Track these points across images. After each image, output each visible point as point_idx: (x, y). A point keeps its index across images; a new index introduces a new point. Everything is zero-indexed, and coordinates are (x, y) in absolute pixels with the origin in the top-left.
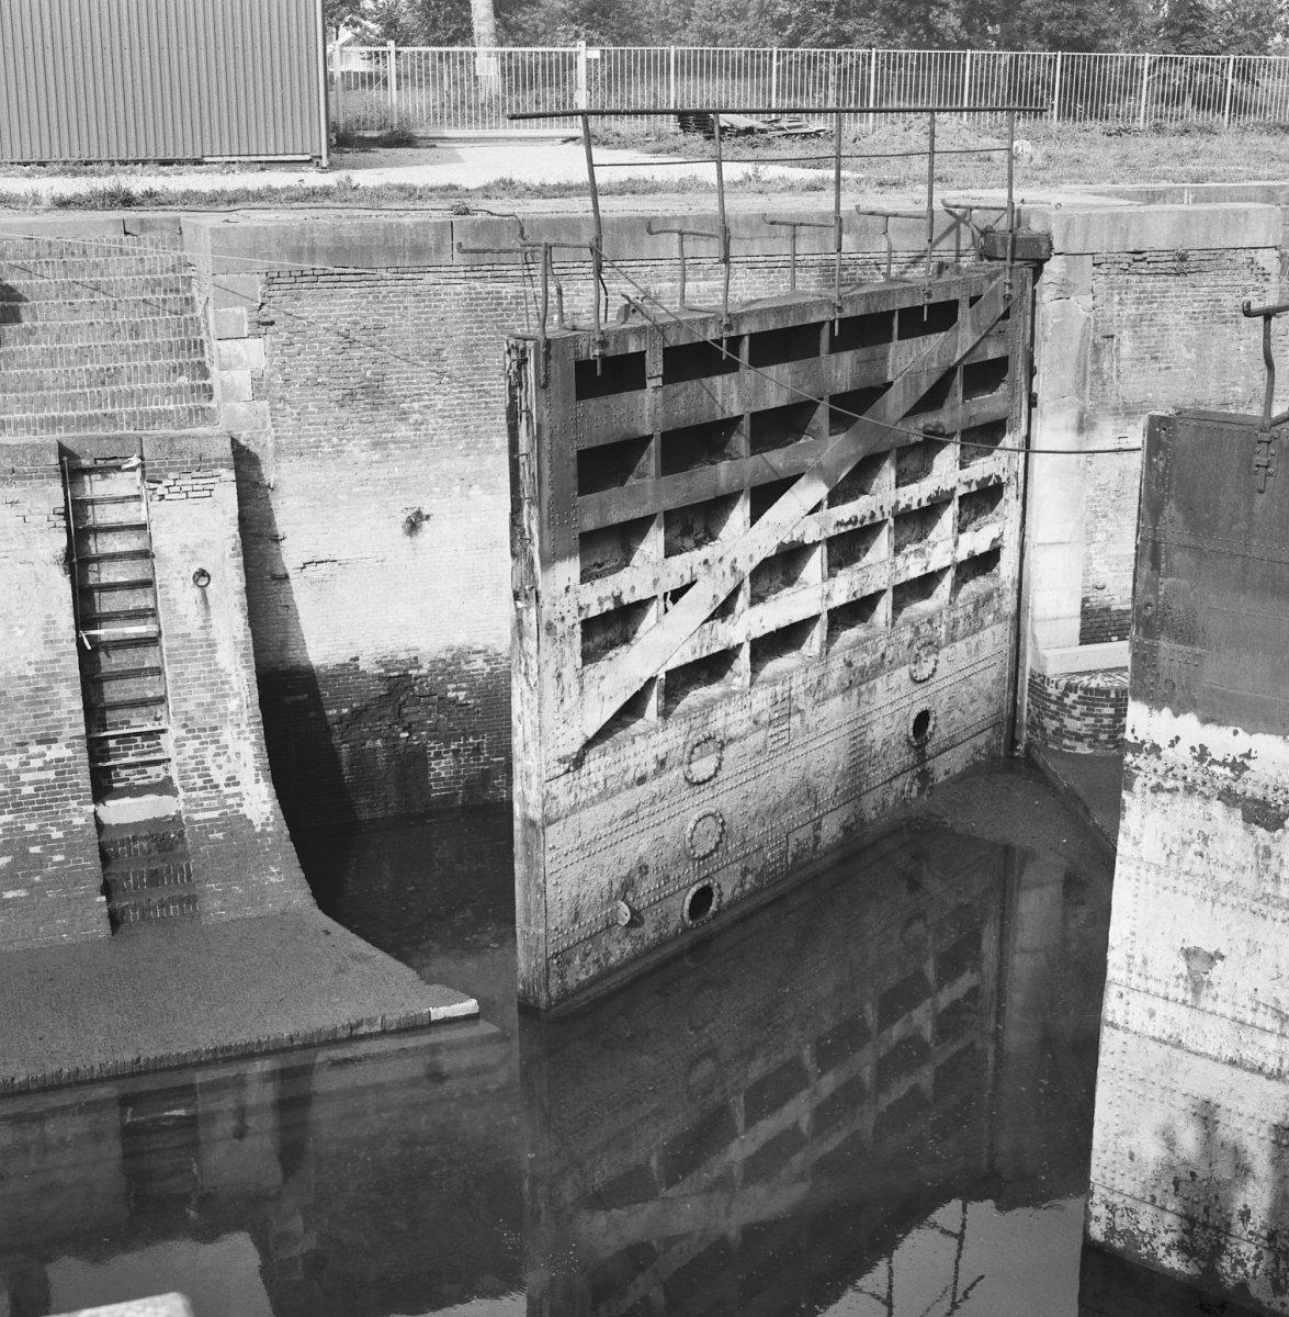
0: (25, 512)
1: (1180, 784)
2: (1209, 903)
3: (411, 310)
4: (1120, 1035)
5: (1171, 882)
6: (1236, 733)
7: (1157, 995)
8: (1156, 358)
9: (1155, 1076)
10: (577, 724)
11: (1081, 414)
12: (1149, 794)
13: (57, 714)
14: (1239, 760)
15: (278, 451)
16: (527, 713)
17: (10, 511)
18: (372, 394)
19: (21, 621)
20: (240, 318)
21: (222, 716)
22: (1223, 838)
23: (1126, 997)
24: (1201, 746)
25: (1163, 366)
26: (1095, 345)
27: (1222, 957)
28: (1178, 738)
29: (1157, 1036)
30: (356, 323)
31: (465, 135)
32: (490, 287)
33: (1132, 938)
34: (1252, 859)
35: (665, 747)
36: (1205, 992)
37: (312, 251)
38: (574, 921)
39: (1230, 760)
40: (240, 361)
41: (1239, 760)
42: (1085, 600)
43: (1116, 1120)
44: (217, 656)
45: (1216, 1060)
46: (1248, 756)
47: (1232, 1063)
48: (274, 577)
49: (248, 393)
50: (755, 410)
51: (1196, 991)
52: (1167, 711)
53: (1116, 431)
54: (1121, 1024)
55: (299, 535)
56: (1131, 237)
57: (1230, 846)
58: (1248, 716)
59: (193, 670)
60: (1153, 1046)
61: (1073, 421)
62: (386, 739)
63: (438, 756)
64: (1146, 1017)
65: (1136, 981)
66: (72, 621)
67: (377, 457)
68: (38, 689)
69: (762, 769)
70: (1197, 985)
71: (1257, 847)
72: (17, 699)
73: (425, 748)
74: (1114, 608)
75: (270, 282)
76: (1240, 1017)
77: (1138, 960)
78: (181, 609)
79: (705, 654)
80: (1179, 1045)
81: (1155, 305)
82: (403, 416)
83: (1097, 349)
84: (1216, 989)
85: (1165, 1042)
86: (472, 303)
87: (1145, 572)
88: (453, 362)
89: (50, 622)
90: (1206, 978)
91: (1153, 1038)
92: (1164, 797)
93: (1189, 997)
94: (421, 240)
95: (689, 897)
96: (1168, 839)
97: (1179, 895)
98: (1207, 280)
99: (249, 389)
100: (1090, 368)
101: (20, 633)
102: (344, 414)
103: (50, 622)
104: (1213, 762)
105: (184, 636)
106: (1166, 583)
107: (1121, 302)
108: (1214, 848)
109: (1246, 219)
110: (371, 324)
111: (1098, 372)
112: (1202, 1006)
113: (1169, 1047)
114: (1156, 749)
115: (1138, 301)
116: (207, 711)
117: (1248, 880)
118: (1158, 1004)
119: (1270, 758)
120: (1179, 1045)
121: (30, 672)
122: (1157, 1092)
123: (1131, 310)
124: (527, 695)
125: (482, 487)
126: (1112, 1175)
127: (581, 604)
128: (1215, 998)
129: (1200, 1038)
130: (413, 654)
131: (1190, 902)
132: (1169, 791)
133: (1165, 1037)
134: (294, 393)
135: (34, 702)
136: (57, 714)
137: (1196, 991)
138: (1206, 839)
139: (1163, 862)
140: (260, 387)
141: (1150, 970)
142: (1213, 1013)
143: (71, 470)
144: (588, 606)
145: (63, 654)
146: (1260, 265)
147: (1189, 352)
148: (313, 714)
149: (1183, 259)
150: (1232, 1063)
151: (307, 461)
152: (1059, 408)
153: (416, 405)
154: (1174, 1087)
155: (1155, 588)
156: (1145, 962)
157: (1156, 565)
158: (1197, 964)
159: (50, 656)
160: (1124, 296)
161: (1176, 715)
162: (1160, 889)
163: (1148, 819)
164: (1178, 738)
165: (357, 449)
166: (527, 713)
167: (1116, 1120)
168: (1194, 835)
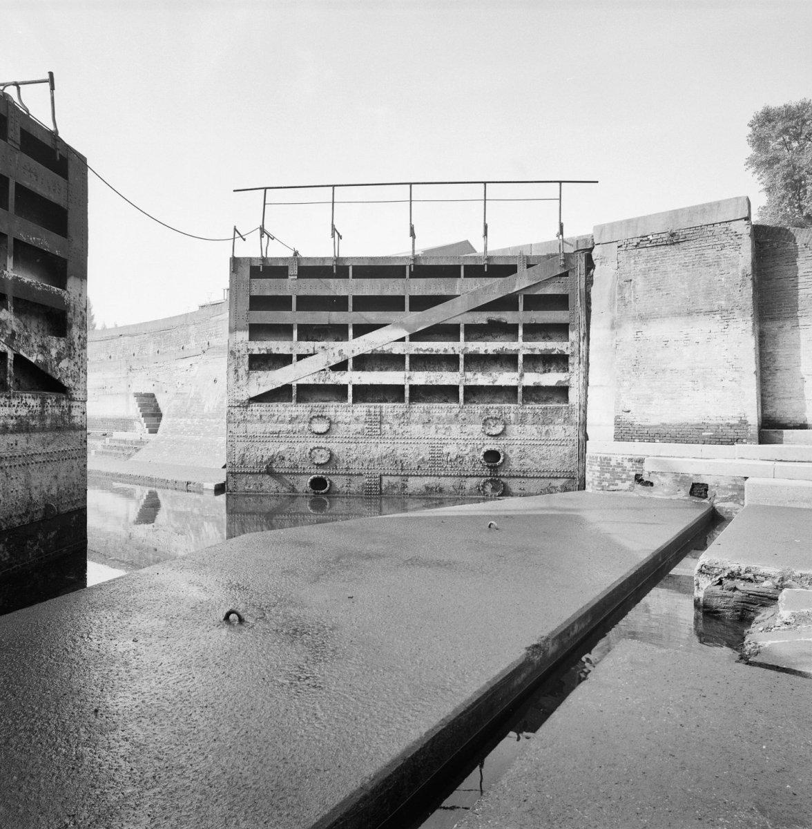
8: (660, 289)
10: (245, 390)
11: (613, 321)
25: (665, 293)
26: (620, 286)
31: (367, 282)
35: (296, 413)
38: (242, 464)
50: (355, 294)
53: (635, 328)
56: (639, 229)
61: (608, 324)
74: (636, 423)
79: (321, 383)
81: (658, 262)
83: (621, 287)
109: (719, 206)
111: (623, 299)
115: (647, 261)
123: (642, 266)
127: (249, 347)
144: (253, 350)
146: (733, 231)
147: (683, 283)
148: (38, 261)
149: (673, 235)
160: (637, 259)
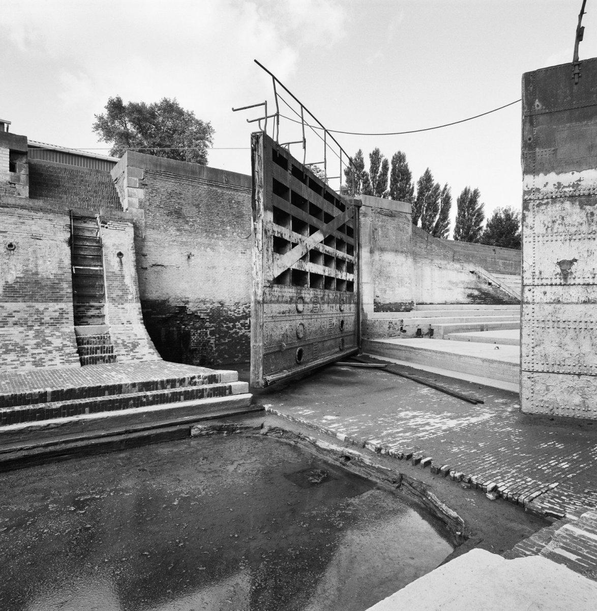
0: (54, 224)
1: (549, 200)
2: (568, 241)
3: (191, 190)
4: (531, 306)
5: (550, 238)
6: (573, 173)
7: (547, 285)
9: (549, 317)
11: (371, 248)
12: (536, 209)
13: (62, 293)
14: (576, 183)
15: (146, 227)
16: (257, 261)
17: (49, 222)
18: (177, 214)
19: (49, 259)
20: (136, 181)
21: (126, 300)
22: (571, 215)
23: (532, 290)
24: (558, 183)
27: (576, 260)
28: (547, 183)
29: (548, 301)
30: (173, 191)
32: (214, 188)
33: (534, 265)
34: (585, 219)
36: (569, 277)
37: (160, 165)
39: (571, 184)
40: (135, 195)
41: (576, 183)
42: (375, 300)
43: (532, 341)
44: (125, 280)
45: (577, 303)
46: (580, 180)
47: (585, 302)
48: (142, 268)
49: (137, 205)
51: (565, 278)
52: (541, 175)
54: (531, 301)
55: (154, 255)
57: (575, 217)
58: (578, 165)
59: (116, 284)
60: (546, 306)
61: (369, 250)
62: (177, 327)
63: (194, 334)
64: (542, 295)
65: (537, 282)
66: (70, 262)
67: (178, 234)
68: (54, 283)
69: (313, 317)
70: (565, 275)
71: (587, 214)
72: (45, 286)
73: (189, 332)
75: (146, 172)
76: (586, 282)
77: (537, 273)
78: (112, 264)
80: (559, 302)
82: (187, 222)
83: (373, 232)
84: (575, 274)
85: (552, 303)
86: (209, 192)
87: (528, 127)
88: (203, 209)
89: (61, 261)
90: (569, 271)
91: (547, 303)
92: (543, 207)
93: (562, 281)
94: (194, 169)
95: (298, 351)
96: (546, 223)
97: (554, 242)
98: (397, 219)
99: (138, 204)
100: (372, 237)
101: (49, 263)
102: (169, 218)
103: (61, 261)
104: (564, 187)
105: (113, 272)
106: (536, 130)
107: (378, 221)
108: (568, 220)
110: (178, 192)
111: (374, 238)
112: (569, 283)
113: (554, 305)
114: (538, 190)
116: (121, 298)
117: (584, 228)
118: (548, 289)
119: (588, 177)
120: (559, 302)
121: (52, 277)
122: (551, 324)
124: (258, 254)
125: (211, 248)
126: (532, 365)
128: (574, 278)
129: (568, 297)
130: (187, 300)
131: (560, 243)
132: (545, 204)
133: (552, 301)
134: (152, 208)
135: (52, 287)
136: (62, 293)
137: (565, 278)
138: (563, 218)
139: (544, 232)
140: (141, 205)
141: (543, 276)
142: (574, 284)
143: (75, 218)
145: (65, 273)
150: (585, 302)
151: (155, 231)
152: (365, 246)
153: (191, 220)
154: (558, 319)
155: (532, 132)
156: (540, 273)
157: (531, 123)
158: (564, 267)
159: (60, 272)
161: (546, 175)
162: (545, 242)
163: (537, 218)
164: (547, 183)
165: (172, 230)
166: (257, 261)
167: (532, 341)
168: (558, 217)
